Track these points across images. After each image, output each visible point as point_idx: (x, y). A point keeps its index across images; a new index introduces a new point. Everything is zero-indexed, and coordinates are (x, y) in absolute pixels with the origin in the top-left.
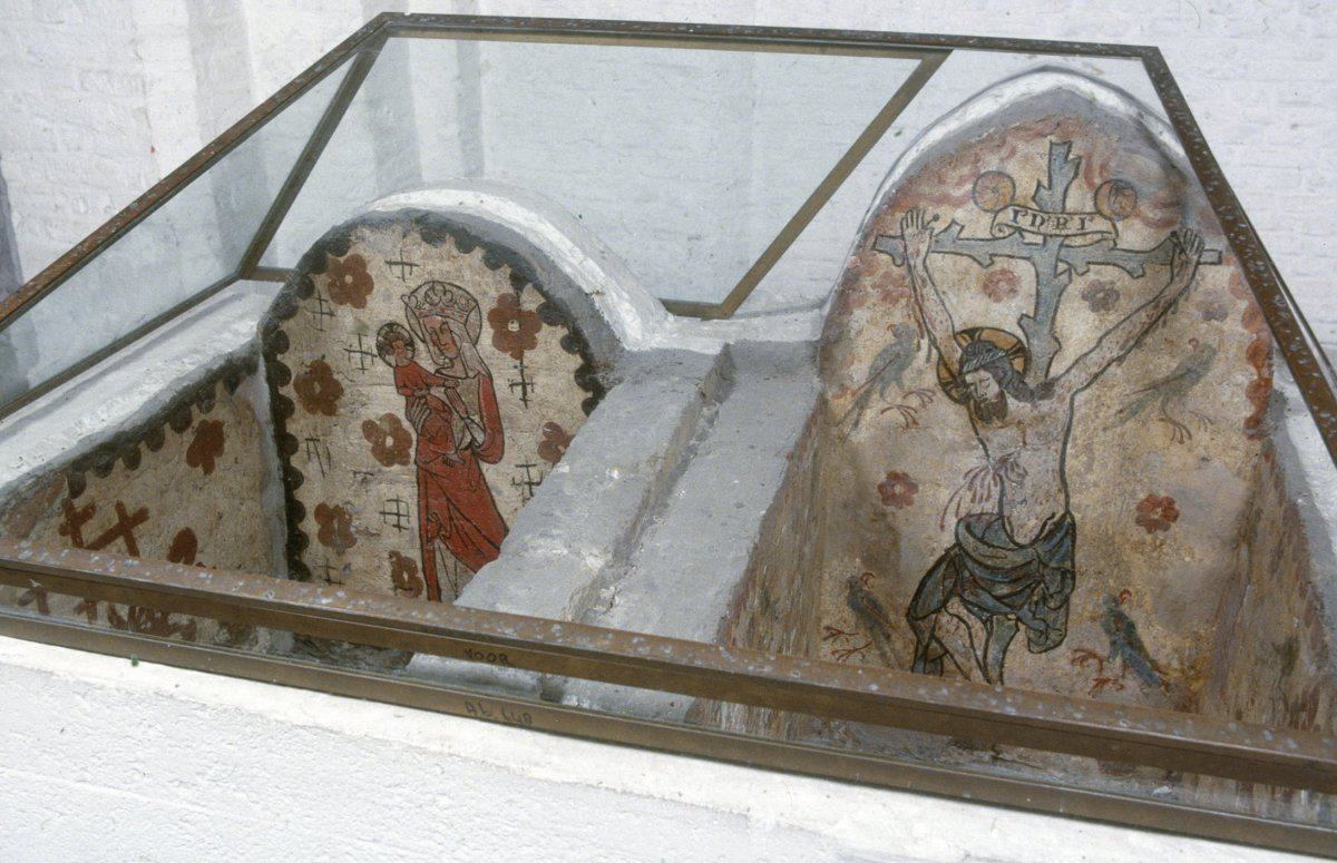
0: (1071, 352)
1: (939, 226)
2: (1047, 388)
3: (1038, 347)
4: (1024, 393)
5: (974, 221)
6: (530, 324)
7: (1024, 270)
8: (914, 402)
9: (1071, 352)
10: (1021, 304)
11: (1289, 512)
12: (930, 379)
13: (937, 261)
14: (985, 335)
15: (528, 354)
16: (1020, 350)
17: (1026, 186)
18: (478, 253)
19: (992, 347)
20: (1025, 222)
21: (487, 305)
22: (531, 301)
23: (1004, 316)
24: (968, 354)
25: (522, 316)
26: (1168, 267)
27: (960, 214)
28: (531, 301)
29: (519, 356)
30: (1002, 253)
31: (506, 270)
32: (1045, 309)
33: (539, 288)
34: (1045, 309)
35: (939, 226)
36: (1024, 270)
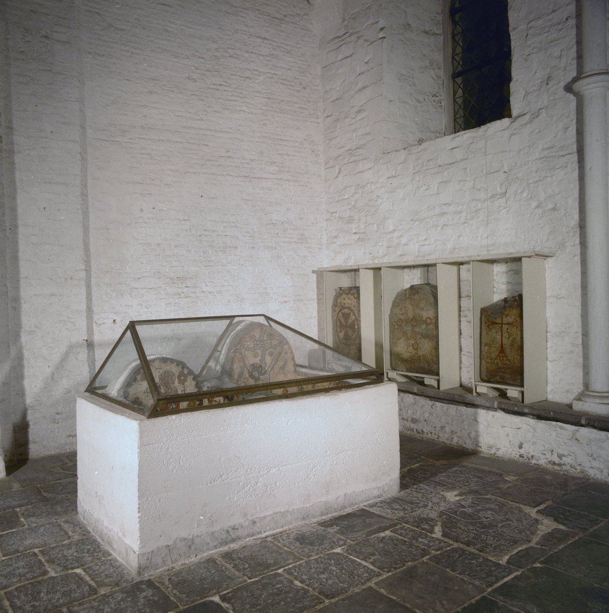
0: (268, 365)
1: (246, 346)
2: (265, 373)
3: (263, 365)
4: (263, 374)
5: (250, 344)
6: (186, 376)
7: (259, 352)
8: (245, 380)
9: (268, 365)
10: (259, 358)
11: (427, 552)
12: (247, 376)
13: (246, 353)
14: (255, 365)
15: (185, 384)
16: (261, 366)
17: (258, 337)
18: (175, 364)
19: (256, 367)
20: (258, 343)
21: (177, 374)
22: (186, 371)
23: (257, 360)
24: (253, 369)
25: (184, 375)
26: (430, 268)
27: (248, 343)
28: (186, 371)
29: (183, 384)
30: (458, 373)
31: (181, 366)
32: (263, 360)
33: (188, 368)
34: (263, 360)
35: (246, 346)
36: (259, 352)
